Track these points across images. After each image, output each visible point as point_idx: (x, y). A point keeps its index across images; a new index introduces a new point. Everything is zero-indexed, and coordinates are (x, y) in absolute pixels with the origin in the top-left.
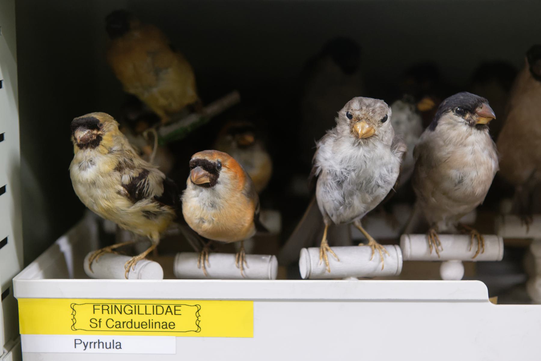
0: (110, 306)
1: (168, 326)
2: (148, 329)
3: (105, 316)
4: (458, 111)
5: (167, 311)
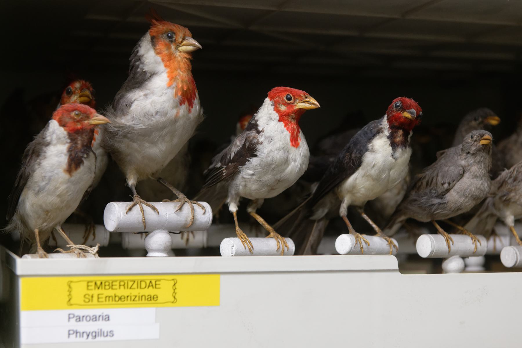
0: (126, 282)
1: (152, 298)
2: (126, 302)
3: (96, 292)
4: (69, 90)
5: (149, 286)
